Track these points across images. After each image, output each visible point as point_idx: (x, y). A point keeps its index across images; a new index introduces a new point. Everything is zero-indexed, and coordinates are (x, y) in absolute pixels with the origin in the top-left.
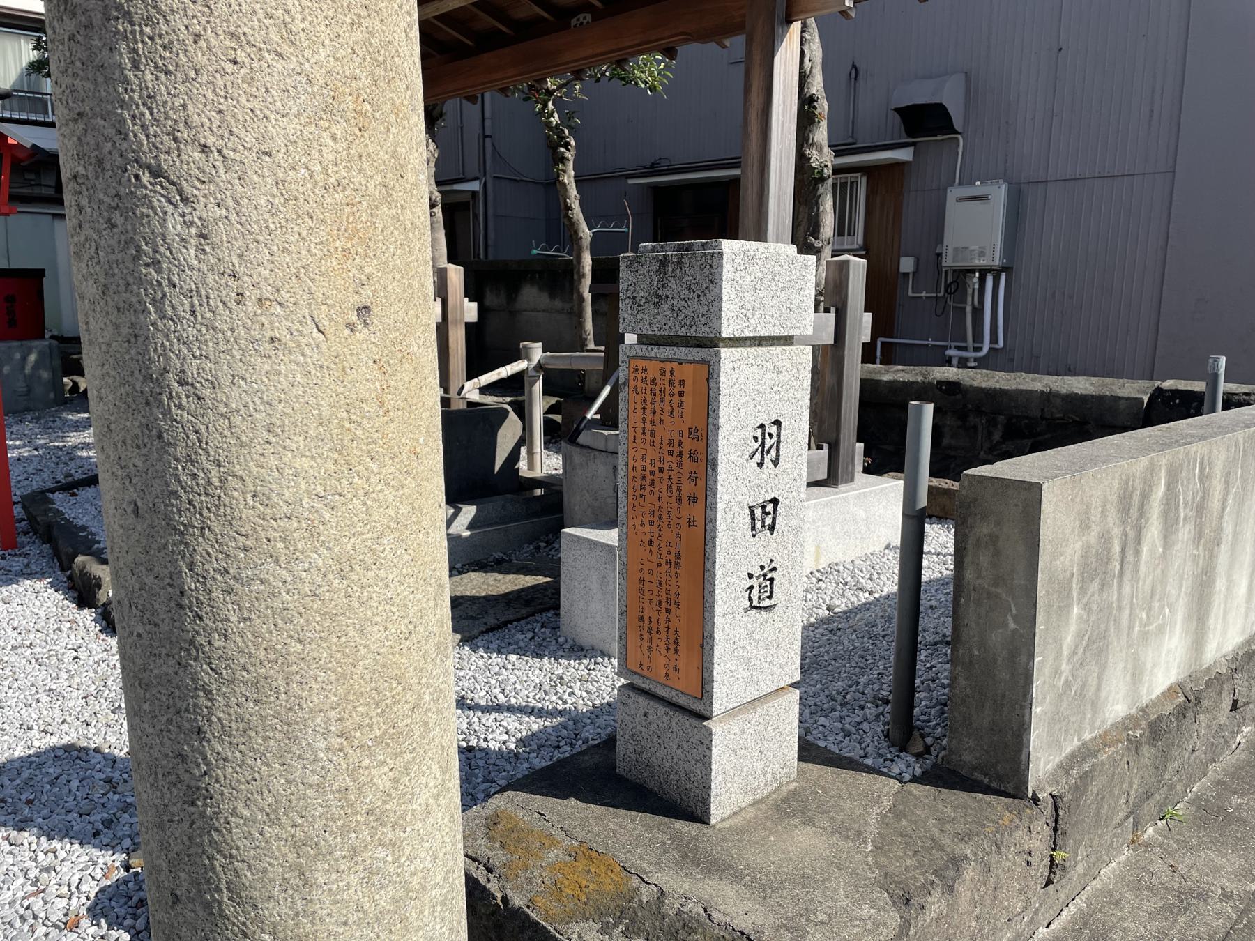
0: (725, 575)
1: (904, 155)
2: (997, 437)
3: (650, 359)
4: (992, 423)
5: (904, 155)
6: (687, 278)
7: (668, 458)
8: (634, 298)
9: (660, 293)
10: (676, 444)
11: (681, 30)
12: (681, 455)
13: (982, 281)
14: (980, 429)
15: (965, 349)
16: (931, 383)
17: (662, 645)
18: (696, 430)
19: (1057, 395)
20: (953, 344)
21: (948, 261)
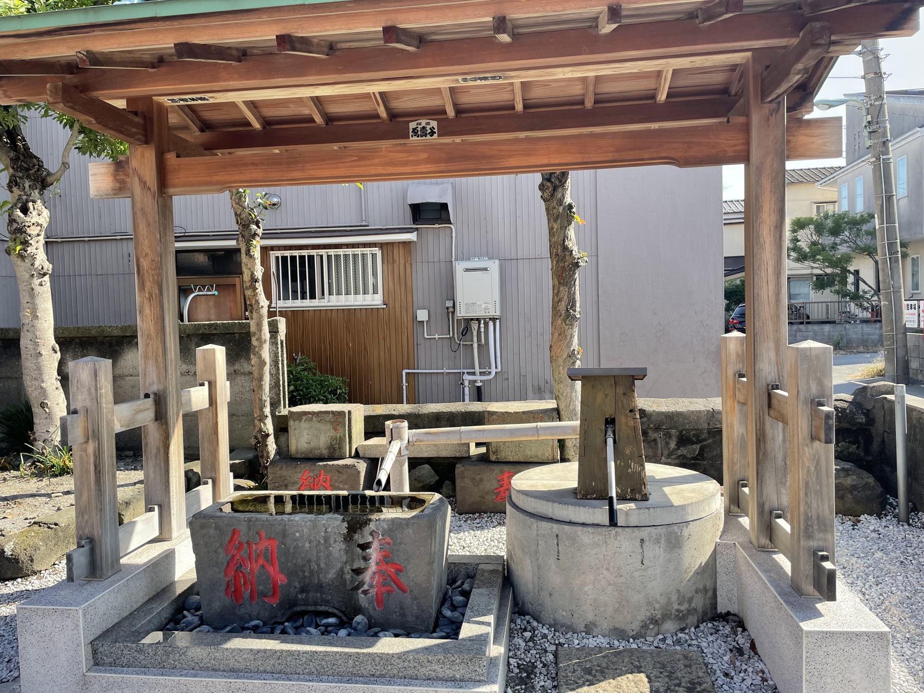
0: (860, 625)
1: (412, 237)
2: (673, 445)
4: (668, 435)
5: (412, 237)
11: (664, 155)
13: (486, 324)
14: (659, 441)
15: (474, 374)
20: (465, 371)
21: (462, 312)
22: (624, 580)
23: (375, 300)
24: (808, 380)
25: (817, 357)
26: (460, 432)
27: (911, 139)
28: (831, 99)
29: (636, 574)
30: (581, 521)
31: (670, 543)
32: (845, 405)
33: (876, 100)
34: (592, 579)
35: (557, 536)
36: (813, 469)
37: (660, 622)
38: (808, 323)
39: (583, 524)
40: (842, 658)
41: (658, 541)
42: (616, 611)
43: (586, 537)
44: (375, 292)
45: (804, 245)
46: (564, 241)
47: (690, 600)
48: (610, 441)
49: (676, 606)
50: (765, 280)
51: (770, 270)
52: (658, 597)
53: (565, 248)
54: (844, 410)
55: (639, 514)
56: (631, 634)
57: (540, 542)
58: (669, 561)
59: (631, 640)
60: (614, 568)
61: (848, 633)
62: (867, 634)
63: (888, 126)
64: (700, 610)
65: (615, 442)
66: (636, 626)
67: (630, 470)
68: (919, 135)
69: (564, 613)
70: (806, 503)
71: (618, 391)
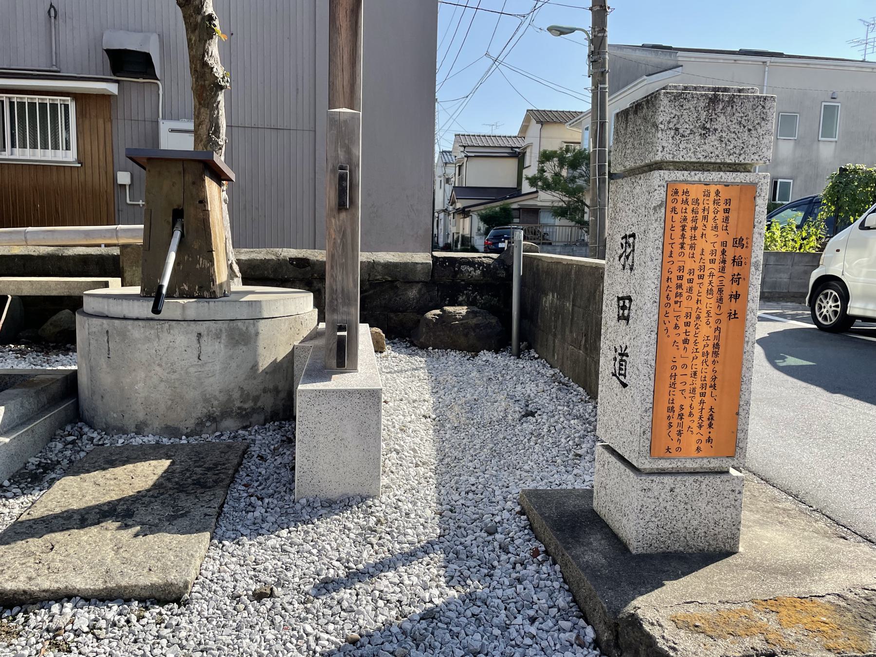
3: (693, 183)
5: (112, 88)
6: (737, 114)
7: (708, 266)
8: (677, 129)
9: (708, 126)
10: (719, 253)
12: (724, 262)
16: (284, 260)
17: (695, 426)
18: (741, 239)
19: (379, 264)
22: (178, 376)
23: (69, 156)
24: (336, 147)
25: (345, 121)
26: (25, 233)
27: (639, 86)
28: (564, 26)
29: (192, 370)
30: (135, 315)
31: (233, 339)
32: (491, 261)
33: (599, 32)
34: (143, 375)
35: (107, 332)
36: (339, 241)
37: (218, 419)
38: (543, 244)
39: (137, 319)
40: (335, 417)
41: (218, 336)
42: (169, 408)
43: (136, 331)
44: (68, 148)
45: (548, 175)
46: (204, 56)
47: (256, 399)
48: (177, 234)
49: (238, 404)
50: (340, 67)
51: (346, 57)
52: (217, 393)
53: (205, 64)
54: (489, 265)
55: (198, 308)
56: (185, 431)
57: (91, 341)
58: (231, 357)
59: (184, 437)
60: (167, 364)
61: (341, 391)
62: (359, 392)
63: (607, 57)
64: (269, 410)
65: (182, 236)
66: (191, 423)
67: (198, 266)
68: (645, 82)
69: (115, 415)
70: (332, 276)
71: (186, 178)
